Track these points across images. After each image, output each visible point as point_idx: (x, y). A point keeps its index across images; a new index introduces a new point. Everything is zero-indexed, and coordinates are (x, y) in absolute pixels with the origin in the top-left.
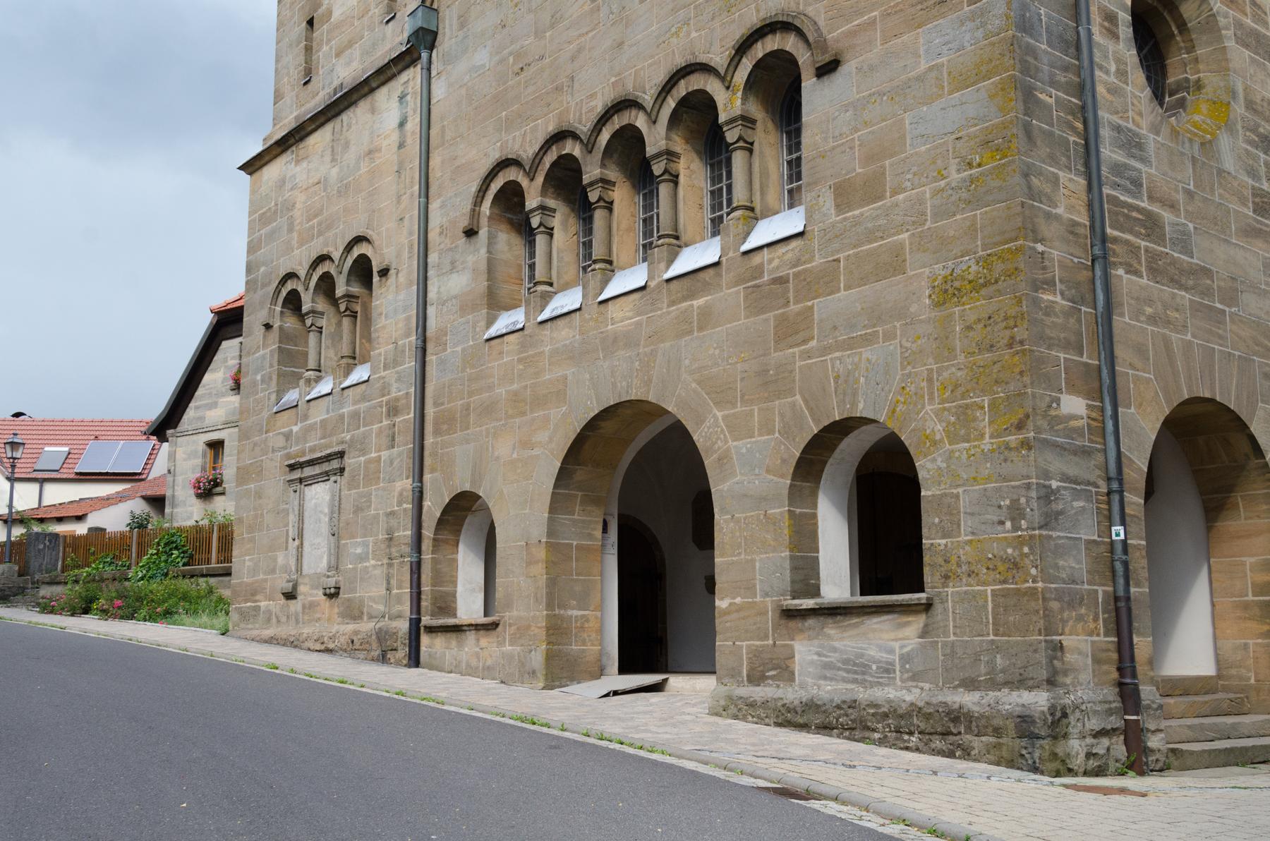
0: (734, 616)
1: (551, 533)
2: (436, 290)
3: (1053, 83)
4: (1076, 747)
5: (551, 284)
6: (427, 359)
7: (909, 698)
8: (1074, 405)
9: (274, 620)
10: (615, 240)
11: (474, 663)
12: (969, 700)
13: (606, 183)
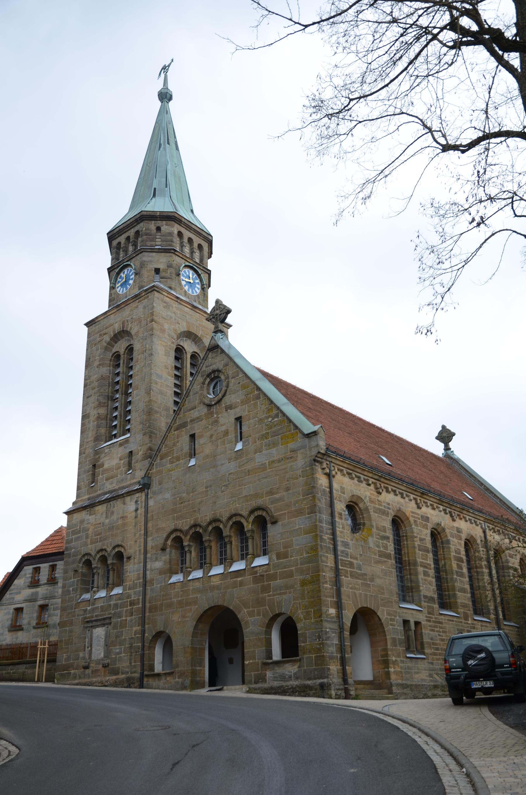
1: (192, 644)
3: (327, 534)
5: (191, 568)
7: (296, 683)
12: (309, 682)
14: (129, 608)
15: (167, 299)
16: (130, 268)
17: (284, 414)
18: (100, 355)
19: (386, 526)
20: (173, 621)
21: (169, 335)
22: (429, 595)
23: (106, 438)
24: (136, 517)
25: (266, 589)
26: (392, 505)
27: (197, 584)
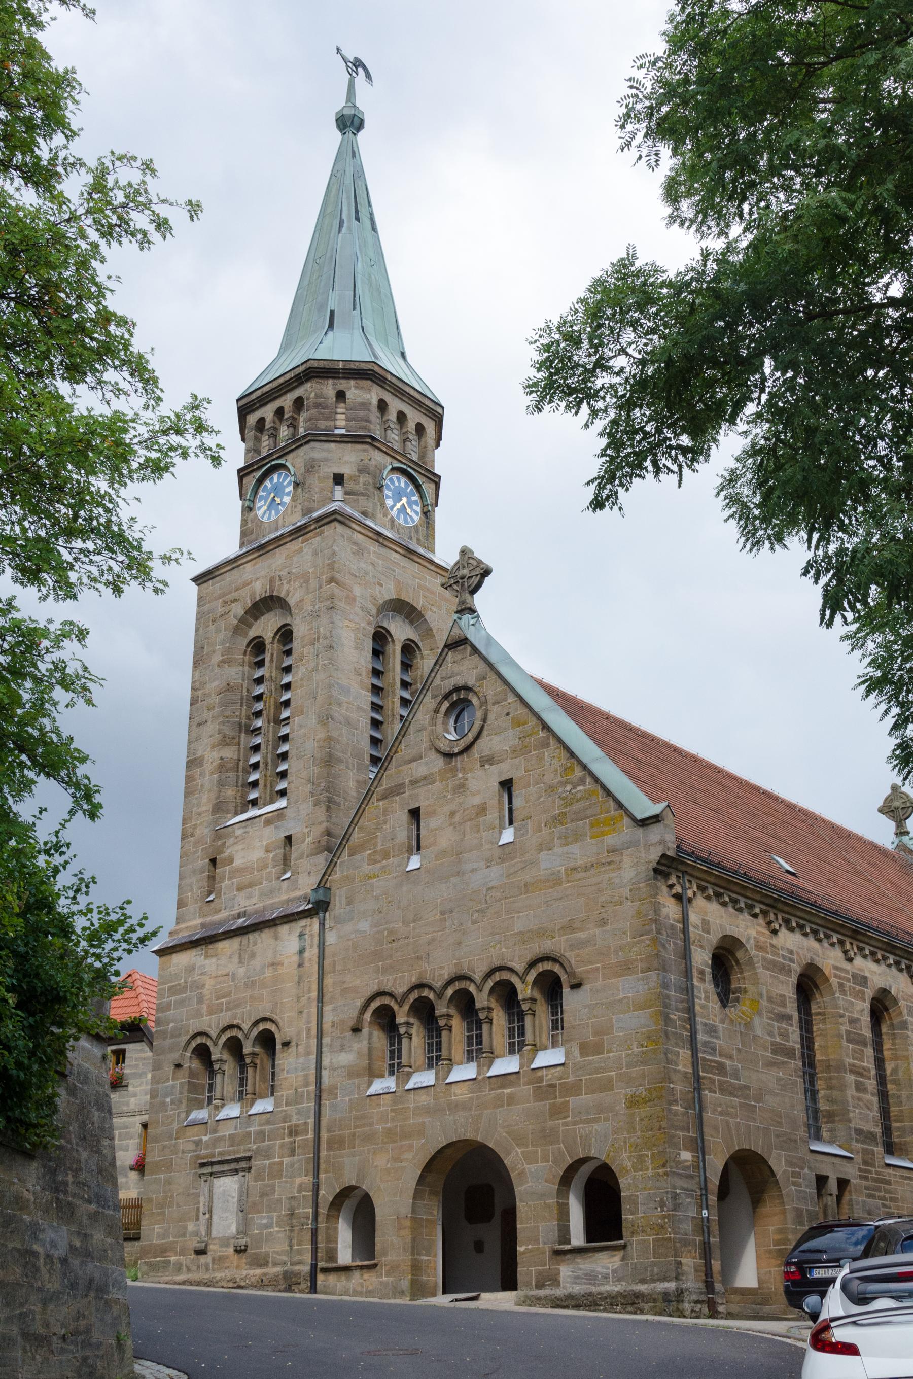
0: (528, 1255)
1: (413, 1212)
2: (328, 1060)
3: (677, 1010)
4: (687, 1306)
5: (411, 1067)
6: (322, 1103)
7: (616, 1289)
8: (686, 1156)
9: (184, 1269)
10: (454, 1047)
11: (359, 1289)
12: (643, 1288)
13: (449, 1016)
14: (287, 1140)
15: (360, 536)
16: (284, 472)
17: (596, 780)
18: (223, 643)
19: (787, 995)
20: (376, 1167)
21: (362, 608)
22: (865, 1129)
23: (236, 806)
24: (301, 965)
25: (558, 1111)
26: (798, 954)
27: (424, 1097)
